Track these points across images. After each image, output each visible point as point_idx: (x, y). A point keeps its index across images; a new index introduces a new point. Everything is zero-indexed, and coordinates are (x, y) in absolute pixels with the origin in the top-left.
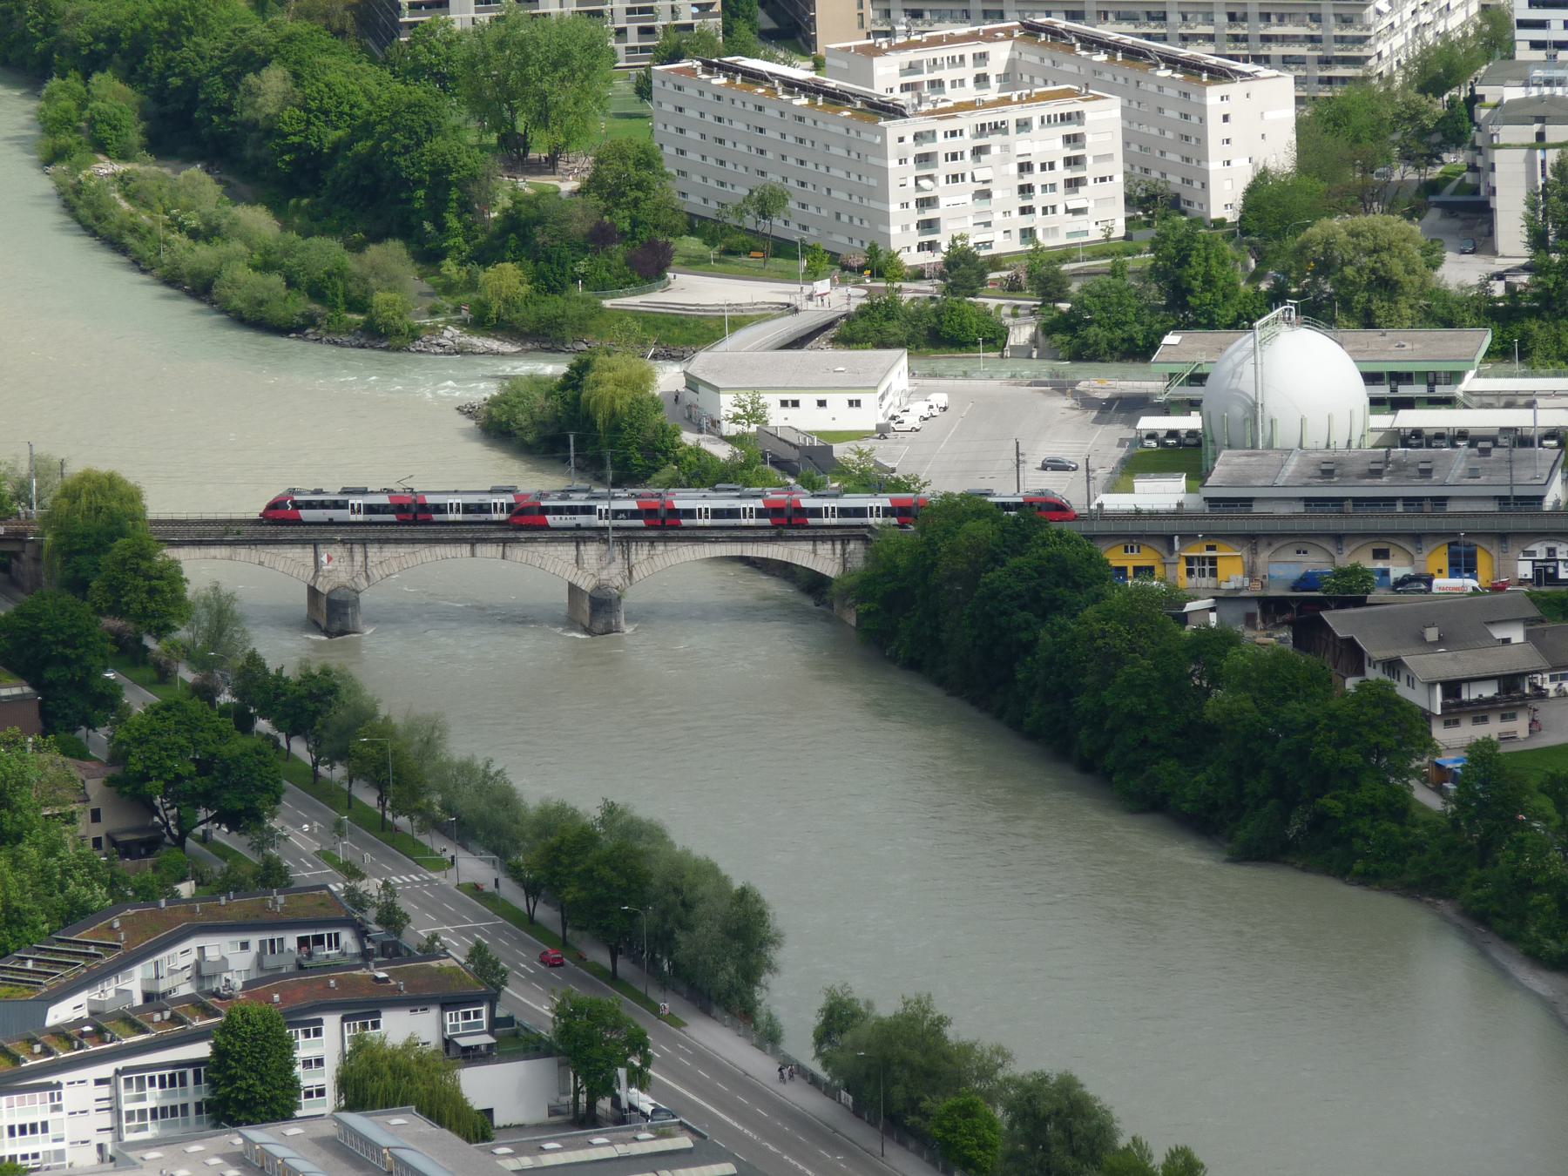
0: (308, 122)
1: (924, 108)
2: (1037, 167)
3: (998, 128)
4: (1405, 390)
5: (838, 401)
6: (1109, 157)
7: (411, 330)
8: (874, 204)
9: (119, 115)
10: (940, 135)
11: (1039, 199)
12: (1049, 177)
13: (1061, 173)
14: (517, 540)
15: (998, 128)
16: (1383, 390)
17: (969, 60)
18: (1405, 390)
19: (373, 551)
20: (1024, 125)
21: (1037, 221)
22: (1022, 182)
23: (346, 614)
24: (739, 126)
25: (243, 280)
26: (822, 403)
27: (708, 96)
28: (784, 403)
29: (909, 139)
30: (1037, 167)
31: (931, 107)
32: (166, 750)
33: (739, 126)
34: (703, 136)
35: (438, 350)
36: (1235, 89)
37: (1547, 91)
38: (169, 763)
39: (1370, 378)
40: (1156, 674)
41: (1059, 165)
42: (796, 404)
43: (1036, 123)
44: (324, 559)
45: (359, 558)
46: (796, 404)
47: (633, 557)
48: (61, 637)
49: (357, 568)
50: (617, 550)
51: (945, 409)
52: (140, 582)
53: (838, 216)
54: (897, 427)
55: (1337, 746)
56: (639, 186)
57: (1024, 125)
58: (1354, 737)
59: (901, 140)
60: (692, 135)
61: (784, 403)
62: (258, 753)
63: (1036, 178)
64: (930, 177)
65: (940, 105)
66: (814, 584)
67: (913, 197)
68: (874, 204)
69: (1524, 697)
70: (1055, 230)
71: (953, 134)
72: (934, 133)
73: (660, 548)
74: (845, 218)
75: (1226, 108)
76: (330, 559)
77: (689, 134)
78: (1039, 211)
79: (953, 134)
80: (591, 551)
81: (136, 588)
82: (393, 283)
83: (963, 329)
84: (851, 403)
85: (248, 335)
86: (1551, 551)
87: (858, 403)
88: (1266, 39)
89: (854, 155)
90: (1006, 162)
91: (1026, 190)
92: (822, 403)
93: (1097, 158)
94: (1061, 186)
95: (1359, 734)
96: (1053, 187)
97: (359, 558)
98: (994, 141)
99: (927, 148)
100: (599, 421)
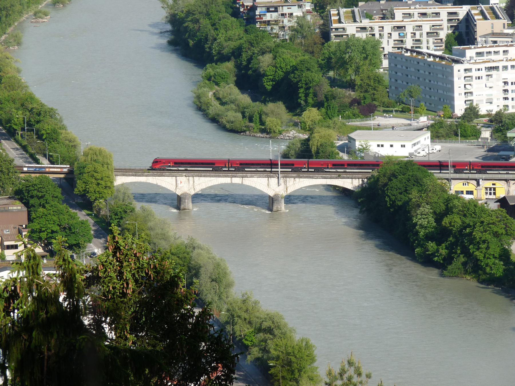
0: (276, 72)
1: (471, 62)
2: (510, 84)
5: (387, 144)
8: (449, 94)
10: (473, 70)
15: (496, 68)
17: (501, 52)
19: (196, 179)
20: (505, 68)
22: (504, 88)
23: (185, 202)
25: (232, 115)
26: (392, 146)
27: (404, 60)
28: (378, 146)
29: (462, 71)
30: (510, 84)
31: (474, 62)
33: (413, 70)
35: (288, 138)
38: (49, 225)
42: (382, 146)
43: (509, 67)
44: (179, 182)
46: (382, 146)
47: (288, 184)
49: (191, 186)
50: (282, 181)
51: (440, 151)
52: (93, 180)
53: (440, 99)
54: (418, 155)
55: (482, 232)
57: (505, 68)
58: (488, 229)
59: (459, 71)
60: (399, 74)
61: (378, 146)
64: (470, 85)
65: (477, 61)
66: (344, 192)
68: (449, 94)
71: (479, 70)
72: (471, 69)
73: (297, 179)
74: (442, 100)
76: (181, 182)
77: (398, 74)
78: (510, 99)
79: (479, 70)
81: (92, 183)
83: (465, 131)
84: (402, 146)
87: (404, 146)
89: (445, 77)
90: (498, 80)
92: (392, 146)
95: (490, 228)
98: (493, 72)
99: (469, 74)
100: (313, 150)
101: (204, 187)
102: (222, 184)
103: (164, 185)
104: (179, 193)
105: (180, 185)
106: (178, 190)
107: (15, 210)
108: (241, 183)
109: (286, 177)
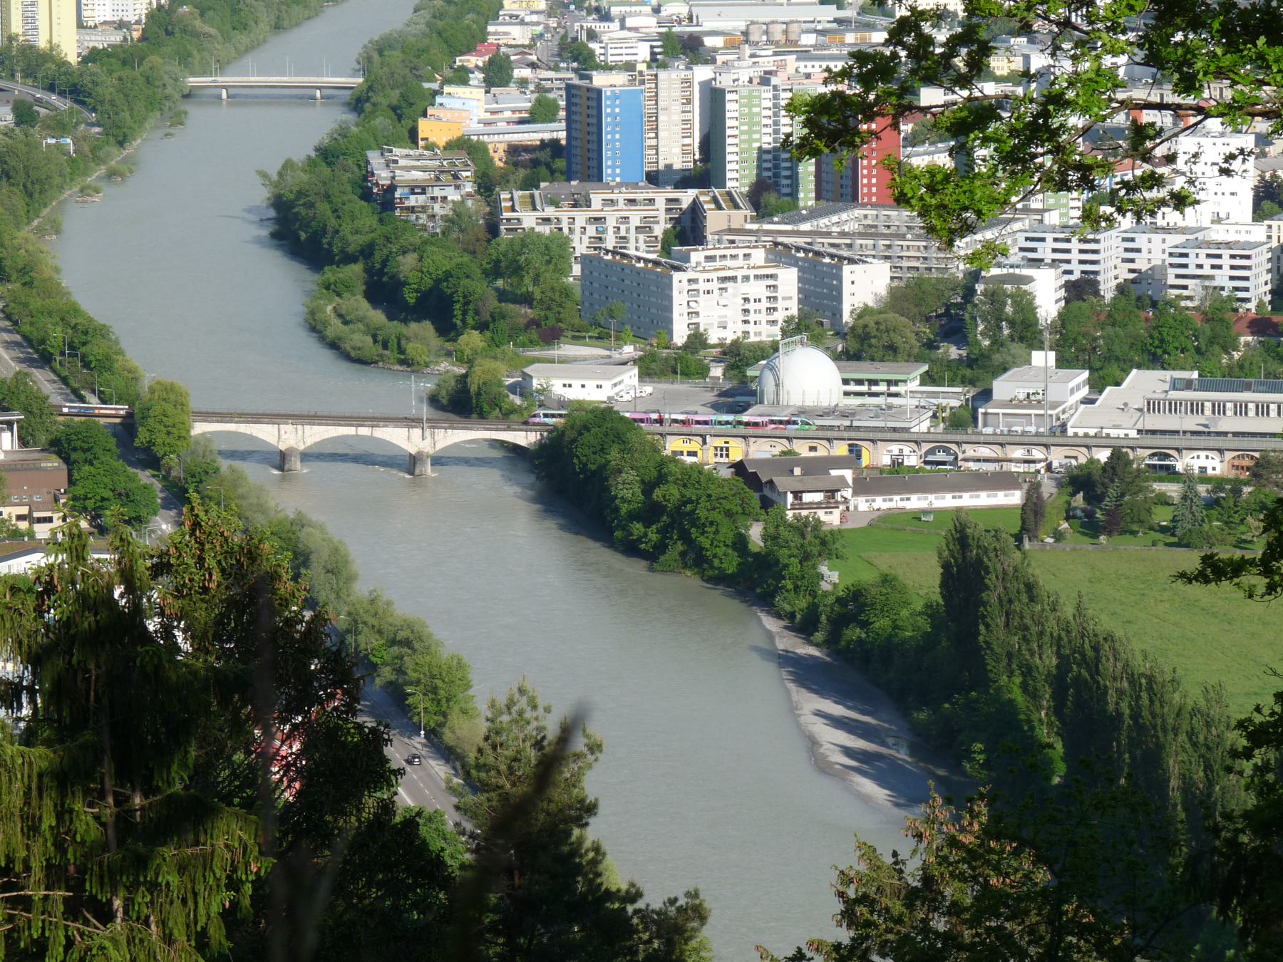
3: (734, 279)
4: (874, 389)
5: (591, 384)
6: (790, 298)
10: (701, 281)
11: (752, 317)
12: (758, 306)
13: (765, 304)
15: (734, 279)
16: (853, 388)
17: (741, 257)
18: (874, 389)
20: (746, 278)
21: (751, 328)
26: (583, 386)
33: (615, 279)
36: (858, 268)
37: (1011, 271)
39: (846, 382)
41: (764, 300)
43: (752, 278)
45: (300, 432)
50: (428, 432)
52: (162, 428)
57: (746, 278)
63: (751, 306)
69: (837, 502)
70: (760, 333)
75: (853, 277)
80: (416, 432)
85: (358, 366)
86: (901, 450)
88: (901, 257)
90: (735, 296)
91: (746, 311)
92: (583, 386)
93: (784, 299)
94: (764, 311)
96: (760, 312)
97: (300, 432)
98: (729, 285)
99: (694, 287)
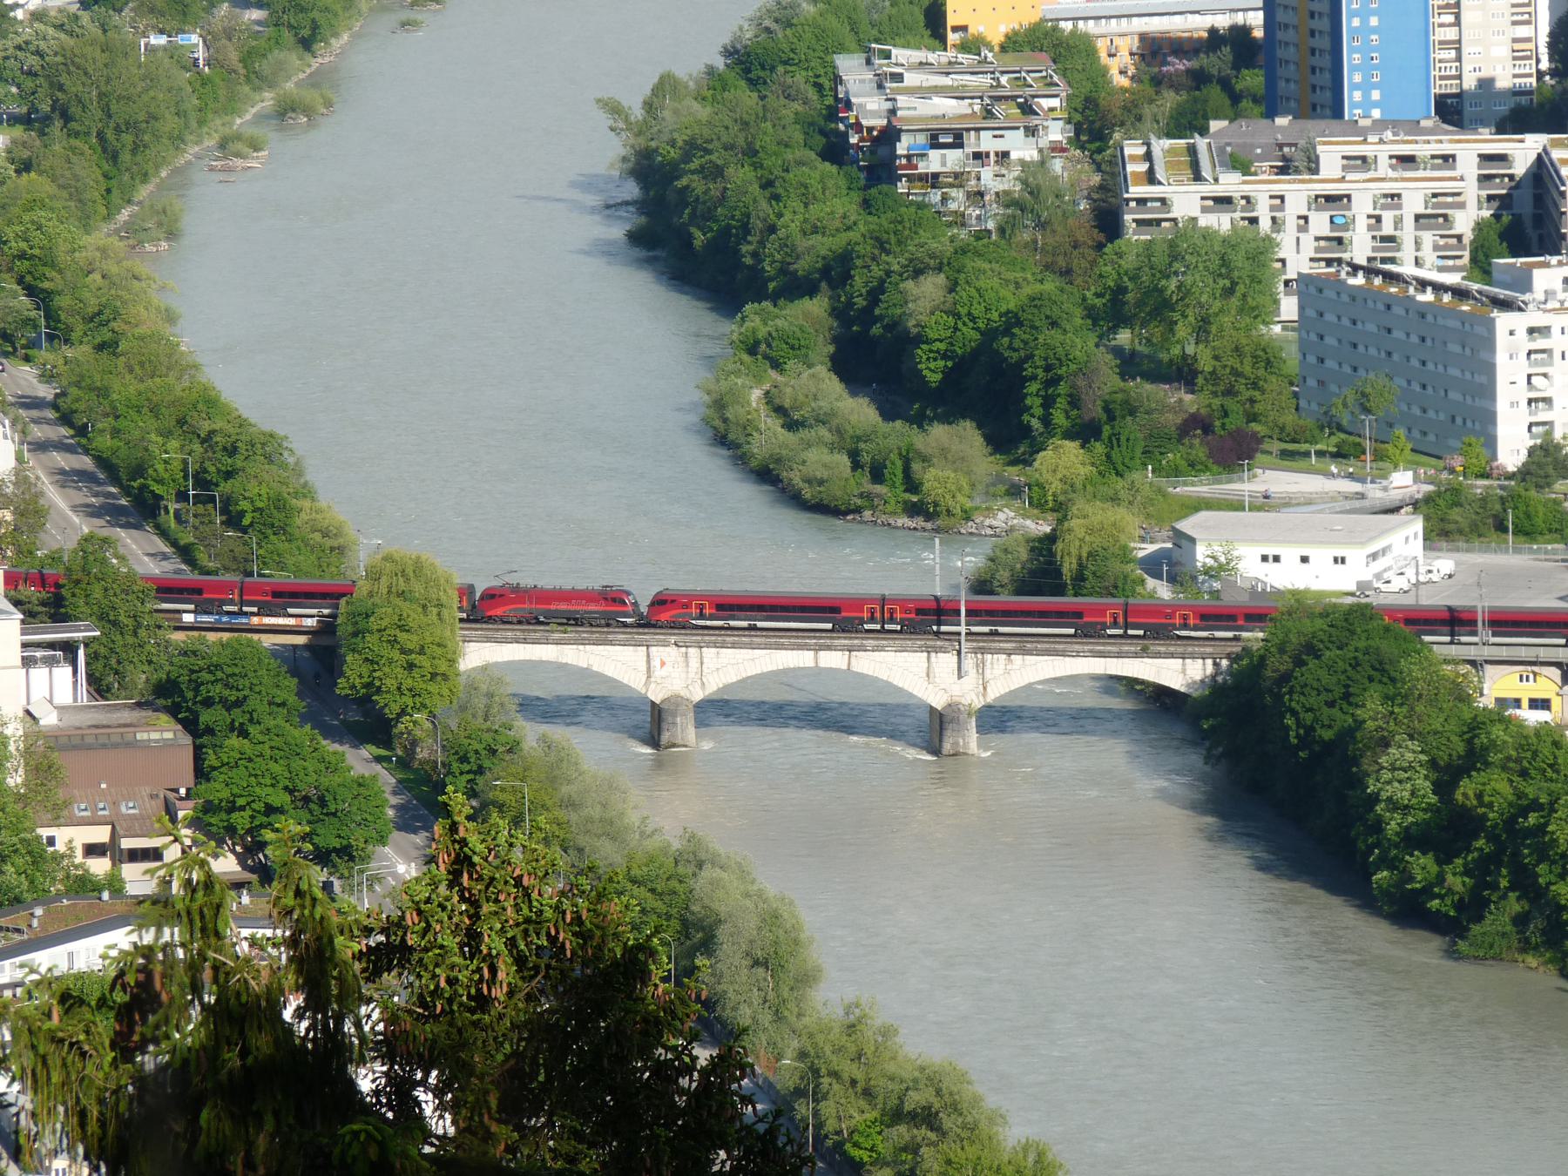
0: (956, 329)
1: (1549, 306)
5: (1290, 554)
7: (964, 511)
8: (1478, 402)
9: (799, 334)
14: (863, 649)
19: (709, 653)
23: (675, 724)
24: (1371, 327)
25: (821, 461)
26: (1305, 560)
27: (1345, 298)
28: (1265, 558)
29: (1522, 334)
31: (1558, 305)
32: (256, 776)
33: (1371, 327)
34: (1340, 341)
38: (258, 790)
40: (1423, 757)
42: (1277, 559)
44: (656, 663)
46: (1277, 559)
48: (219, 674)
49: (692, 675)
51: (1450, 576)
52: (396, 655)
53: (1453, 418)
54: (1384, 587)
56: (1255, 385)
59: (1512, 333)
61: (1265, 558)
62: (360, 785)
67: (1524, 394)
73: (1017, 658)
74: (1459, 421)
76: (663, 664)
82: (958, 462)
84: (1336, 560)
85: (804, 518)
87: (1343, 561)
92: (1305, 560)
99: (1541, 343)
100: (1065, 570)
101: (732, 678)
102: (786, 671)
103: (610, 671)
104: (656, 696)
105: (658, 672)
106: (653, 686)
107: (156, 741)
108: (845, 667)
109: (983, 651)
